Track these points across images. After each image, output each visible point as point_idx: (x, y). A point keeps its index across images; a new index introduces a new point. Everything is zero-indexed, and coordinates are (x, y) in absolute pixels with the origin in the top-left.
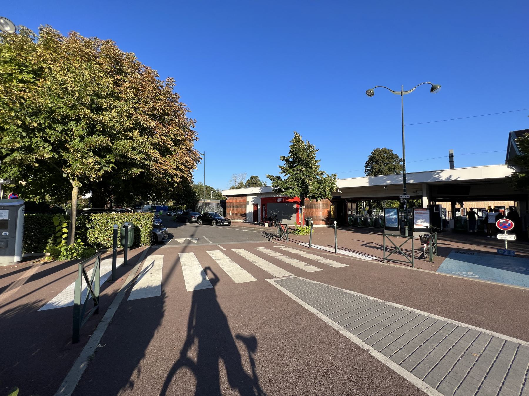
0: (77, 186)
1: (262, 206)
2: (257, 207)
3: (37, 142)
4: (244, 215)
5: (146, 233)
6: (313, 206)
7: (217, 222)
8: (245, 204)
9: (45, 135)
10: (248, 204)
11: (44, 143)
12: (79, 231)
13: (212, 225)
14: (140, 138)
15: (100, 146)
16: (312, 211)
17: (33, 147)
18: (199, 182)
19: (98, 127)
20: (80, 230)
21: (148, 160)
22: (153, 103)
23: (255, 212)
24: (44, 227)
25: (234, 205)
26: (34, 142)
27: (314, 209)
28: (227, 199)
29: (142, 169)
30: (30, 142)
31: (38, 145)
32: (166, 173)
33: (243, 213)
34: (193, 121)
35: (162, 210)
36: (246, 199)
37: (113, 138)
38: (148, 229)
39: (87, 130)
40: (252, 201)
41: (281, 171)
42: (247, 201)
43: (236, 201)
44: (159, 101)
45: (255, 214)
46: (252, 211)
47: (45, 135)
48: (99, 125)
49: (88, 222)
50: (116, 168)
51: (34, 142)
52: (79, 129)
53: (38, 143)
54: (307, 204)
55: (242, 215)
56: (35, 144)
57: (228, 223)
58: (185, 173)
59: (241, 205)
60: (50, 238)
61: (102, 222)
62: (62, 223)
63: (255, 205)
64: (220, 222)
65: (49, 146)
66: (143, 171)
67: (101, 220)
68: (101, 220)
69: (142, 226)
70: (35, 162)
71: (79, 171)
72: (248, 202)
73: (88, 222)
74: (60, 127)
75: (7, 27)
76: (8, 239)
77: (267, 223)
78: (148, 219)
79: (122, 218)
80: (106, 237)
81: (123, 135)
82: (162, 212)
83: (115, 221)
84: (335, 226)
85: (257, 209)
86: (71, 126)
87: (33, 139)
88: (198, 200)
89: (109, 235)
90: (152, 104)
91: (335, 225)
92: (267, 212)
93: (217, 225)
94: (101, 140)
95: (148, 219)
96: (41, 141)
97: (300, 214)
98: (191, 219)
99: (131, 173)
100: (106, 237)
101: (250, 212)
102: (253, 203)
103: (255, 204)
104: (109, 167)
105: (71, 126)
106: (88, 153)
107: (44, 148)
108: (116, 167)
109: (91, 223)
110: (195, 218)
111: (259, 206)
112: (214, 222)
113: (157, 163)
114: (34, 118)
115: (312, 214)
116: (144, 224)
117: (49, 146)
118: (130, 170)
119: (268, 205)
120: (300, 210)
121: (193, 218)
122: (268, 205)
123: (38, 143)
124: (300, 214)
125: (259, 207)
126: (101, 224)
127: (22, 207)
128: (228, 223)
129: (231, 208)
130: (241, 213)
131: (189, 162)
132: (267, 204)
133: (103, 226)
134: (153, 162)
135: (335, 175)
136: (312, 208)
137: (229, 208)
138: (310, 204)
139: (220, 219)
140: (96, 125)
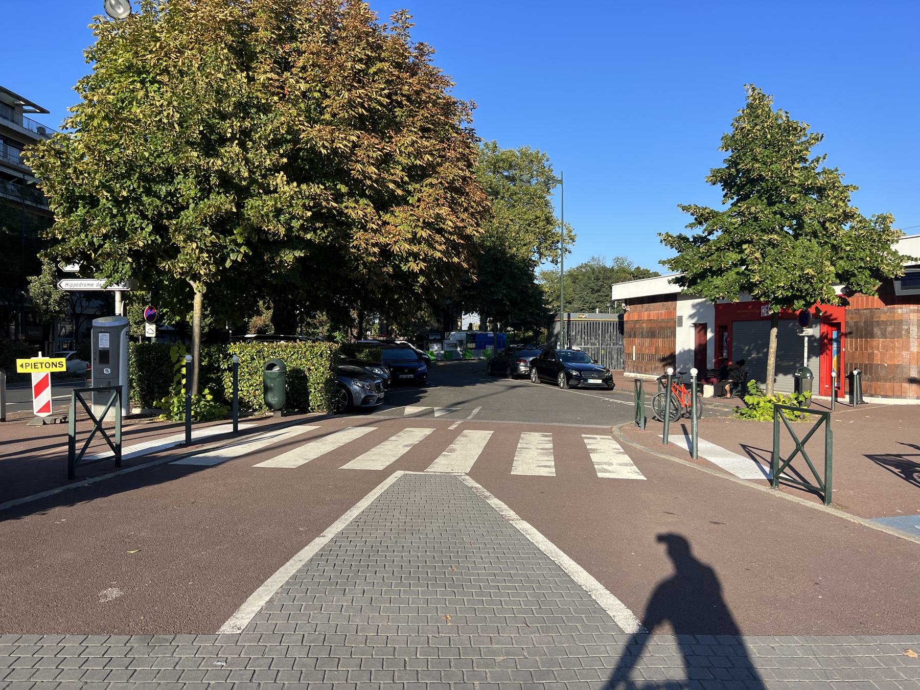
0: (200, 291)
1: (720, 330)
2: (706, 333)
3: (132, 221)
4: (670, 360)
5: (318, 384)
6: (877, 331)
7: (569, 377)
8: (669, 328)
9: (141, 208)
10: (681, 325)
11: (142, 221)
12: (212, 375)
13: (557, 385)
14: (286, 188)
15: (217, 215)
16: (872, 348)
17: (126, 230)
18: (617, 260)
19: (214, 180)
20: (214, 373)
21: (311, 231)
22: (349, 90)
23: (699, 355)
24: (163, 365)
25: (643, 328)
26: (129, 220)
27: (879, 342)
28: (625, 311)
29: (301, 251)
30: (123, 222)
31: (134, 224)
32: (386, 253)
33: (667, 354)
34: (469, 105)
35: (490, 343)
36: (675, 309)
37: (242, 193)
38: (322, 376)
39: (199, 187)
40: (691, 316)
41: (692, 220)
42: (678, 314)
43: (649, 315)
44: (376, 77)
45: (699, 357)
46: (693, 347)
47: (141, 208)
48: (214, 176)
49: (224, 358)
50: (251, 254)
51: (129, 220)
52: (187, 187)
53: (135, 223)
54: (856, 323)
55: (663, 360)
56: (129, 225)
57: (600, 381)
58: (435, 249)
59: (662, 328)
60: (172, 384)
61: (243, 359)
62: (181, 359)
63: (701, 328)
64: (578, 378)
65: (148, 225)
66: (303, 255)
67: (242, 355)
68: (242, 355)
69: (309, 369)
70: (128, 255)
71: (181, 265)
72: (681, 318)
73: (224, 358)
74: (164, 188)
75: (119, 8)
76: (111, 380)
77: (712, 384)
78: (321, 355)
79: (275, 352)
80: (251, 388)
81: (261, 186)
82: (490, 349)
83: (264, 358)
84: (693, 381)
85: (704, 342)
86: (178, 183)
87: (127, 216)
88: (554, 316)
89: (255, 385)
90: (347, 94)
91: (692, 377)
92: (733, 349)
93: (568, 383)
94: (223, 202)
95: (321, 355)
96: (138, 219)
97: (835, 359)
98: (516, 368)
99: (281, 261)
100: (251, 388)
101: (685, 351)
102: (694, 321)
103: (700, 324)
104: (239, 252)
105: (178, 183)
106: (202, 230)
107: (142, 229)
108: (252, 251)
109: (228, 360)
110: (526, 366)
111: (709, 330)
112: (562, 375)
113: (366, 231)
114: (126, 182)
115: (871, 356)
116: (314, 365)
117: (148, 225)
118: (278, 254)
119: (738, 328)
120: (835, 345)
121: (522, 364)
122: (738, 328)
123: (135, 223)
124: (835, 359)
125: (710, 335)
126: (242, 363)
127: (125, 329)
128: (600, 381)
129: (635, 337)
130: (661, 355)
131: (445, 220)
132: (735, 324)
133: (245, 367)
134: (357, 228)
135: (884, 219)
136: (871, 335)
137: (630, 337)
138: (865, 322)
139: (576, 370)
140: (210, 176)
